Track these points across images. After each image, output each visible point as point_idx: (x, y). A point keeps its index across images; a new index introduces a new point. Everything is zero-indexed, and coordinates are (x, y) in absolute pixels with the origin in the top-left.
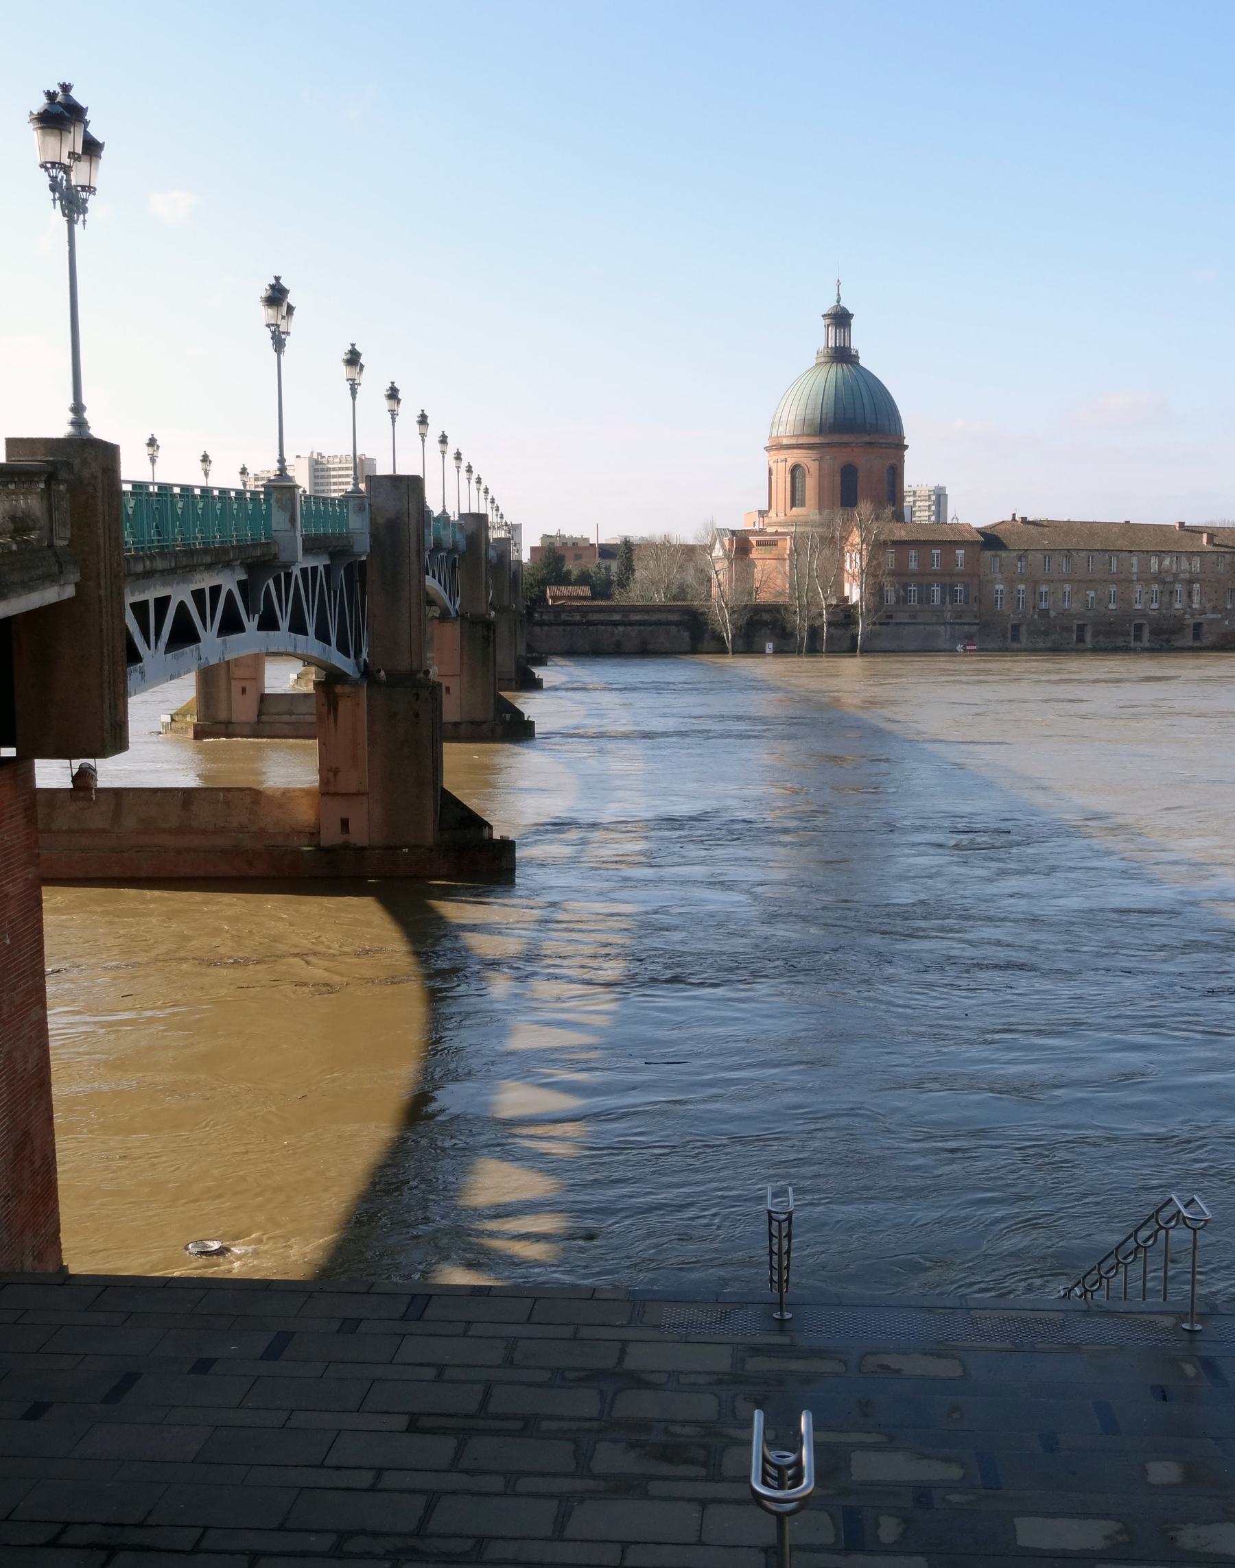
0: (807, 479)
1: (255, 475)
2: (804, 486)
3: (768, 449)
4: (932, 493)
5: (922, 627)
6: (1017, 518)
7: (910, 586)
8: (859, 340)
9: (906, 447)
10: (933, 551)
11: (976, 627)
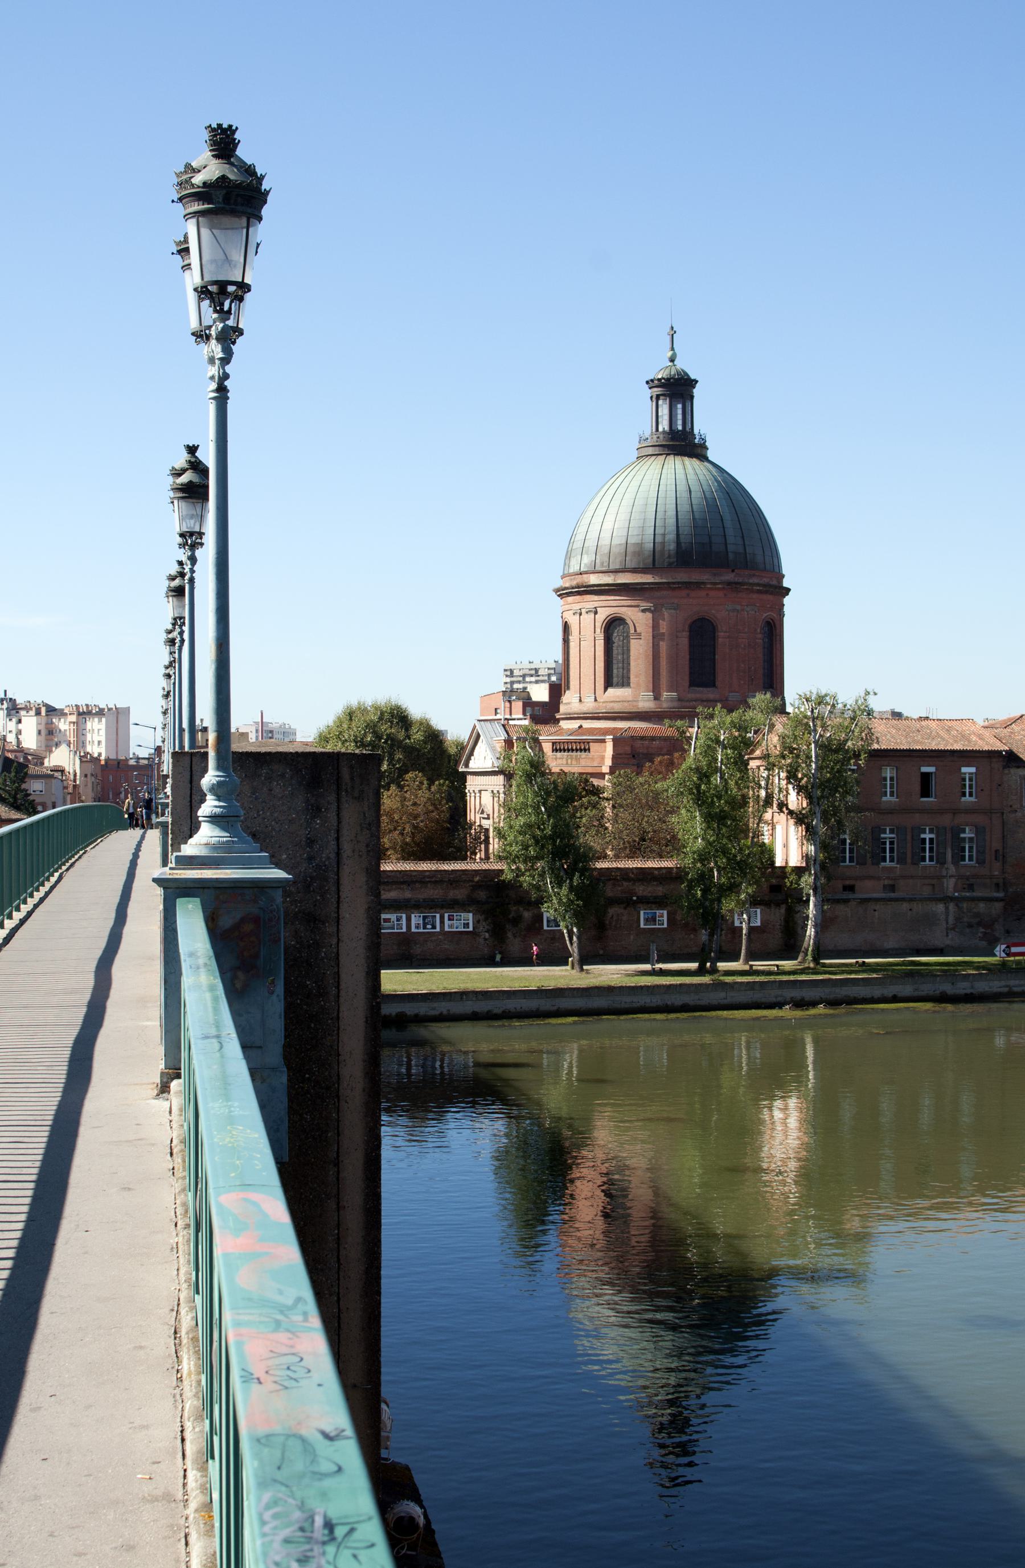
0: (632, 642)
3: (563, 593)
4: (552, 672)
5: (905, 906)
7: (885, 833)
10: (924, 769)
11: (999, 906)
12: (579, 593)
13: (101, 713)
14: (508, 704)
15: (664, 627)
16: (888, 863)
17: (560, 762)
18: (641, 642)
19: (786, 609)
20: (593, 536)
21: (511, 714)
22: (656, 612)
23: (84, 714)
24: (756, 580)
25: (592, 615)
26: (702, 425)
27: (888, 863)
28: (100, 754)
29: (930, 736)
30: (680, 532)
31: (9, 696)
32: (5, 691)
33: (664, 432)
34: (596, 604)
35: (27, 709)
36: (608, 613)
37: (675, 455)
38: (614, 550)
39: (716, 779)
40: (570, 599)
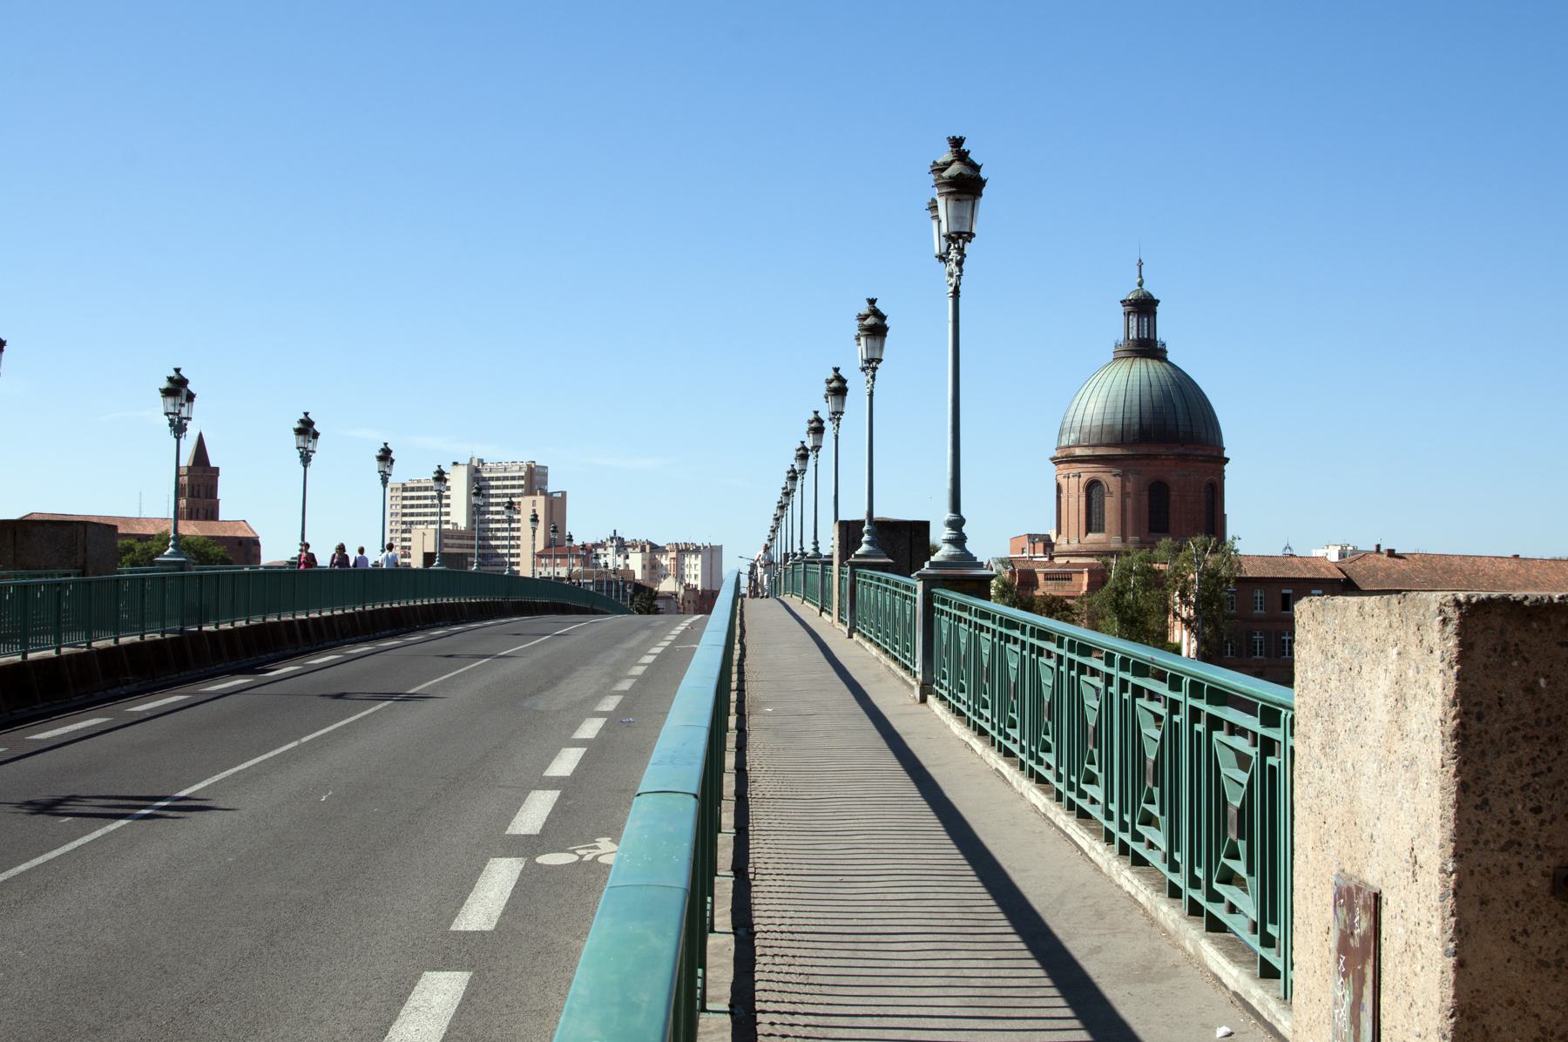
1: (404, 484)
2: (1102, 505)
3: (1057, 461)
6: (1382, 550)
7: (1256, 635)
8: (1165, 332)
9: (1227, 460)
10: (1284, 591)
12: (1067, 462)
13: (697, 550)
14: (1032, 545)
15: (1130, 487)
16: (1258, 657)
17: (1050, 588)
18: (1113, 499)
19: (1226, 474)
20: (1078, 418)
21: (1034, 553)
22: (1123, 476)
23: (683, 551)
24: (1200, 452)
25: (1077, 478)
26: (1163, 334)
27: (1258, 657)
28: (696, 586)
29: (1292, 569)
30: (1143, 416)
31: (618, 535)
32: (615, 531)
33: (1133, 340)
34: (1080, 470)
35: (634, 546)
36: (1088, 477)
37: (1141, 357)
38: (1093, 430)
39: (1130, 596)
40: (1061, 466)
